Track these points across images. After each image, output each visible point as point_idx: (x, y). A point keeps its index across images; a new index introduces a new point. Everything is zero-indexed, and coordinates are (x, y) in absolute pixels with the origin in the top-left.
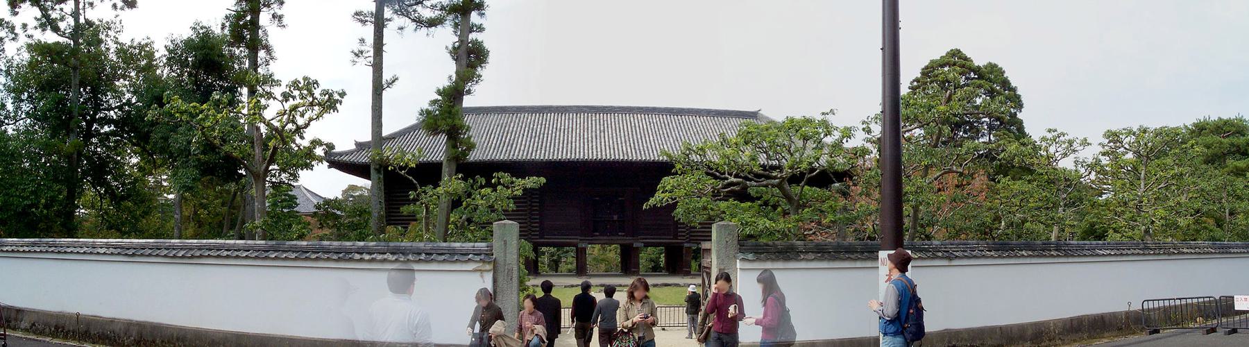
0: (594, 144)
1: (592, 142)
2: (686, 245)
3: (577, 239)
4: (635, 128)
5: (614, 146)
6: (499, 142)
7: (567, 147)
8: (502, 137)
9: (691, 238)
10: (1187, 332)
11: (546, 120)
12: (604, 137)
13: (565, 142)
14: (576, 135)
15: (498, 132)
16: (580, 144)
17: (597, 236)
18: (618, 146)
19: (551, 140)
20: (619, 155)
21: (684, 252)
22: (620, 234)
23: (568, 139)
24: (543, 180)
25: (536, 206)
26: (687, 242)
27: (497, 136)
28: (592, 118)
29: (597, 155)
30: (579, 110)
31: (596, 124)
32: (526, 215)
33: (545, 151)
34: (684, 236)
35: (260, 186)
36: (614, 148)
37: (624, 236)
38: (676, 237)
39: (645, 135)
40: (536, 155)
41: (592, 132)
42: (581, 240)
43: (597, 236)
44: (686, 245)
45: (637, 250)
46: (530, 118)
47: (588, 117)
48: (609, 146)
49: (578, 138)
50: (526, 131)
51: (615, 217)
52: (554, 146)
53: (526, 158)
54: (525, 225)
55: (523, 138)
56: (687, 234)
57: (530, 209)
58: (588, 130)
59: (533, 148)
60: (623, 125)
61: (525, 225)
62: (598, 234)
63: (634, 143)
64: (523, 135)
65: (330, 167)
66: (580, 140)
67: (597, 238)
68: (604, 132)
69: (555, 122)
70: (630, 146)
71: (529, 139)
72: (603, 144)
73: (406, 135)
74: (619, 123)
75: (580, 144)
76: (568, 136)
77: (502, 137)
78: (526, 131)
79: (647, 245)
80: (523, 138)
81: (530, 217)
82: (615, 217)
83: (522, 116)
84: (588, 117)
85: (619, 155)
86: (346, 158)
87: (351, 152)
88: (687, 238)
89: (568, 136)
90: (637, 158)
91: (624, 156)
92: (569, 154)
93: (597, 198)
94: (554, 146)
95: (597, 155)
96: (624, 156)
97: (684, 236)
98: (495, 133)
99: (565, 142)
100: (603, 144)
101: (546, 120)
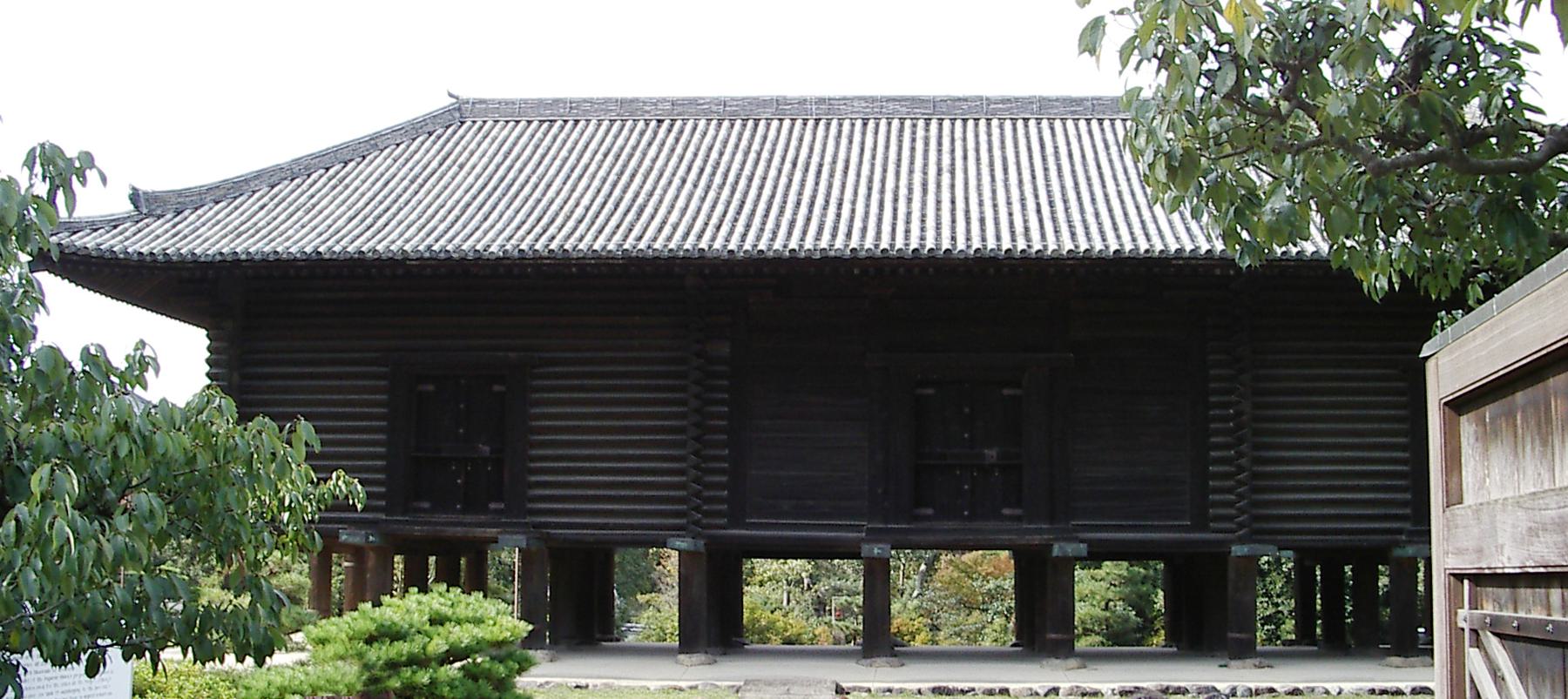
0: (916, 205)
1: (909, 200)
2: (1238, 550)
3: (858, 528)
4: (1057, 158)
5: (982, 212)
6: (600, 200)
7: (824, 215)
8: (614, 185)
9: (1257, 525)
10: (1533, 567)
11: (765, 138)
12: (953, 186)
13: (820, 201)
14: (858, 182)
15: (602, 173)
16: (868, 206)
17: (927, 518)
18: (996, 212)
19: (773, 196)
20: (998, 238)
21: (1231, 575)
22: (1006, 511)
23: (828, 195)
24: (385, 463)
25: (720, 416)
26: (1241, 541)
27: (596, 183)
28: (914, 133)
29: (923, 238)
30: (874, 110)
31: (926, 151)
32: (682, 445)
33: (748, 226)
34: (1230, 518)
35: (1511, 420)
36: (982, 221)
37: (1019, 519)
38: (1201, 524)
39: (1088, 179)
40: (713, 239)
41: (911, 172)
42: (869, 531)
43: (424, 511)
44: (1238, 550)
45: (1067, 566)
46: (711, 132)
47: (901, 130)
48: (967, 212)
49: (862, 190)
50: (695, 170)
51: (991, 454)
52: (782, 212)
53: (680, 247)
54: (682, 493)
55: (679, 190)
56: (1242, 511)
57: (696, 425)
58: (898, 165)
59: (709, 217)
60: (979, 174)
61: (682, 493)
62: (930, 511)
63: (1051, 204)
64: (684, 181)
66: (869, 196)
67: (926, 525)
68: (952, 172)
69: (794, 143)
70: (1039, 211)
71: (699, 192)
72: (946, 205)
73: (555, 130)
74: (1003, 147)
75: (868, 206)
76: (830, 186)
77: (614, 185)
78: (695, 170)
79: (1095, 557)
80: (679, 190)
81: (696, 453)
82: (991, 454)
83: (690, 124)
84: (901, 130)
85: (998, 238)
86: (87, 241)
87: (115, 223)
88: (1241, 526)
89: (830, 186)
90: (1137, 248)
91: (1014, 240)
92: (826, 236)
93: (930, 391)
94: (782, 212)
95: (923, 238)
96: (1014, 240)
97: (1230, 518)
98: (594, 177)
99: (820, 201)
100: (946, 205)
101: (765, 138)
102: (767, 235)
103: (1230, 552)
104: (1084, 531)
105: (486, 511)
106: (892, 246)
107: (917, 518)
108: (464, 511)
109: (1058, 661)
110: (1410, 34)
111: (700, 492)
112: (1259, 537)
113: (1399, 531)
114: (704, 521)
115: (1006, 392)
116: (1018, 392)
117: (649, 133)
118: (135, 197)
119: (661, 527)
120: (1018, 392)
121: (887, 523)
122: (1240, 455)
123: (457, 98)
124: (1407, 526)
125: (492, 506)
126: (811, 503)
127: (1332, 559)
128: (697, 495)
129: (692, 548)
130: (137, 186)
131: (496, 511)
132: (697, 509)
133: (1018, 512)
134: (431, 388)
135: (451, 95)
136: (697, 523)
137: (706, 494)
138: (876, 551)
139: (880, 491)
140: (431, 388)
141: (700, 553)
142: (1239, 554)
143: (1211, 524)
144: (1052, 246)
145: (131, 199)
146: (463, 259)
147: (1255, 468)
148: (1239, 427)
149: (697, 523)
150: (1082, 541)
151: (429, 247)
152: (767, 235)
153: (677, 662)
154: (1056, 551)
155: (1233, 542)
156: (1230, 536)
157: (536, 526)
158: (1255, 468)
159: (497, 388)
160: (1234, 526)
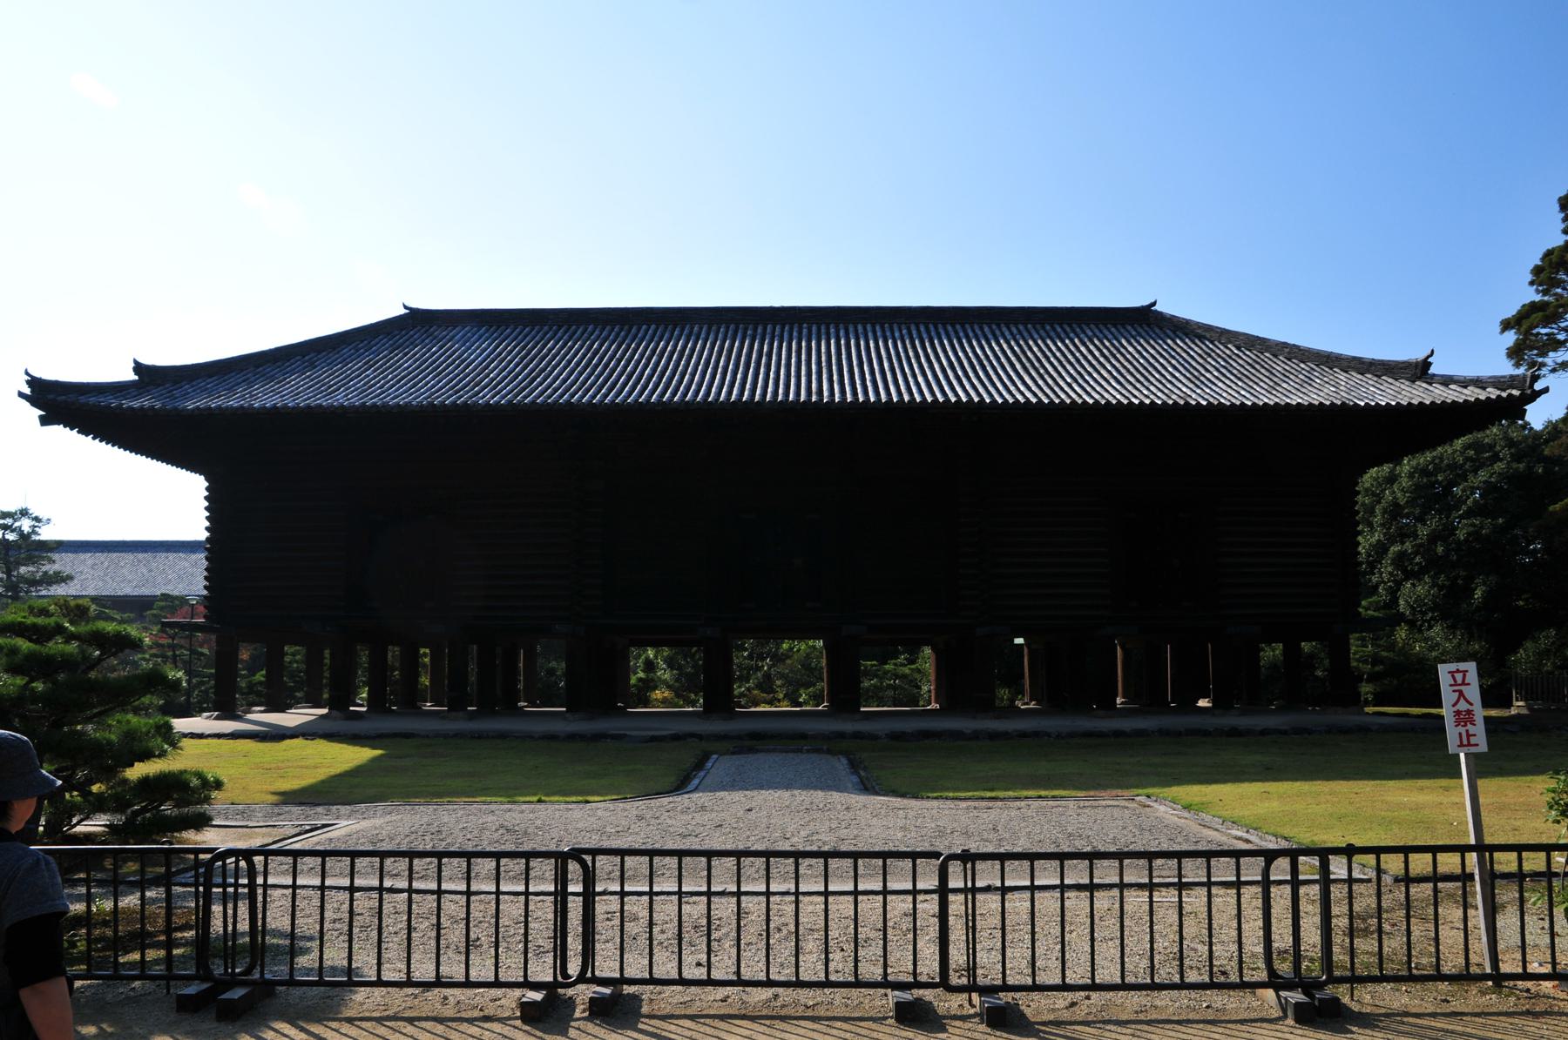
118: (139, 368)
135: (406, 307)
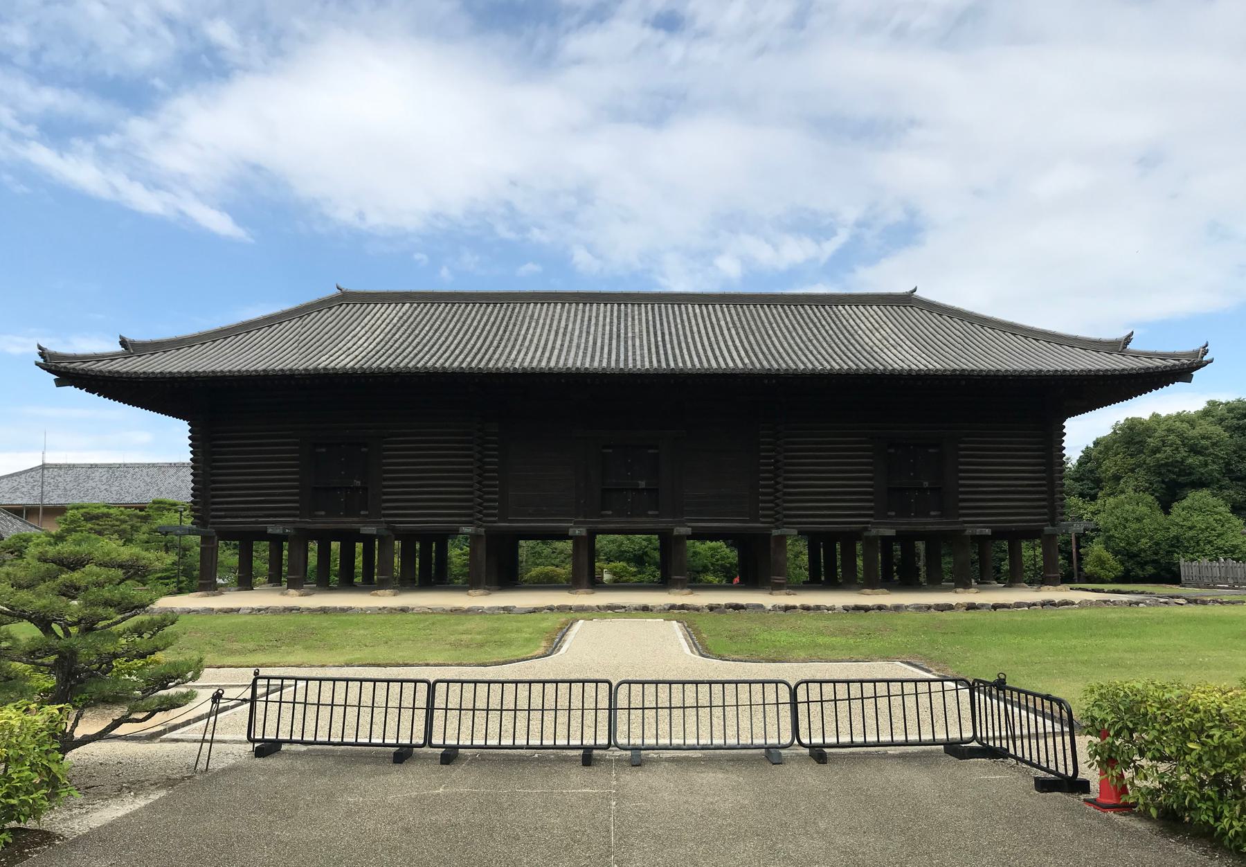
26: (778, 528)
37: (657, 516)
43: (608, 516)
65: (59, 383)
67: (607, 519)
81: (479, 483)
87: (113, 357)
102: (597, 359)
103: (771, 534)
104: (689, 522)
105: (359, 515)
106: (634, 367)
107: (602, 516)
108: (346, 516)
109: (678, 591)
110: (74, 734)
111: (482, 503)
112: (787, 526)
113: (868, 523)
114: (484, 519)
115: (650, 451)
116: (656, 451)
117: (419, 309)
118: (123, 343)
119: (456, 522)
120: (656, 451)
121: (586, 518)
122: (778, 483)
123: (341, 290)
124: (872, 520)
125: (362, 513)
126: (545, 509)
127: (829, 538)
128: (480, 505)
129: (473, 532)
130: (123, 335)
131: (364, 516)
132: (480, 512)
133: (657, 513)
134: (324, 450)
136: (480, 519)
137: (485, 504)
138: (577, 532)
139: (582, 502)
140: (324, 450)
141: (481, 536)
142: (776, 534)
143: (761, 519)
144: (689, 365)
145: (121, 344)
146: (372, 373)
147: (785, 490)
148: (777, 461)
149: (480, 519)
150: (689, 527)
151: (361, 367)
152: (597, 359)
153: (468, 594)
154: (675, 533)
155: (772, 528)
156: (772, 525)
157: (387, 522)
158: (785, 490)
159: (364, 450)
160: (773, 520)
